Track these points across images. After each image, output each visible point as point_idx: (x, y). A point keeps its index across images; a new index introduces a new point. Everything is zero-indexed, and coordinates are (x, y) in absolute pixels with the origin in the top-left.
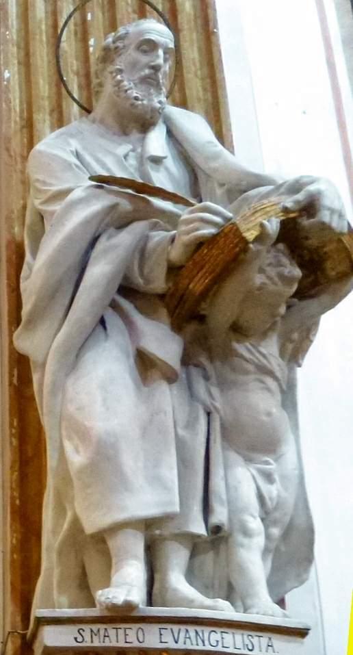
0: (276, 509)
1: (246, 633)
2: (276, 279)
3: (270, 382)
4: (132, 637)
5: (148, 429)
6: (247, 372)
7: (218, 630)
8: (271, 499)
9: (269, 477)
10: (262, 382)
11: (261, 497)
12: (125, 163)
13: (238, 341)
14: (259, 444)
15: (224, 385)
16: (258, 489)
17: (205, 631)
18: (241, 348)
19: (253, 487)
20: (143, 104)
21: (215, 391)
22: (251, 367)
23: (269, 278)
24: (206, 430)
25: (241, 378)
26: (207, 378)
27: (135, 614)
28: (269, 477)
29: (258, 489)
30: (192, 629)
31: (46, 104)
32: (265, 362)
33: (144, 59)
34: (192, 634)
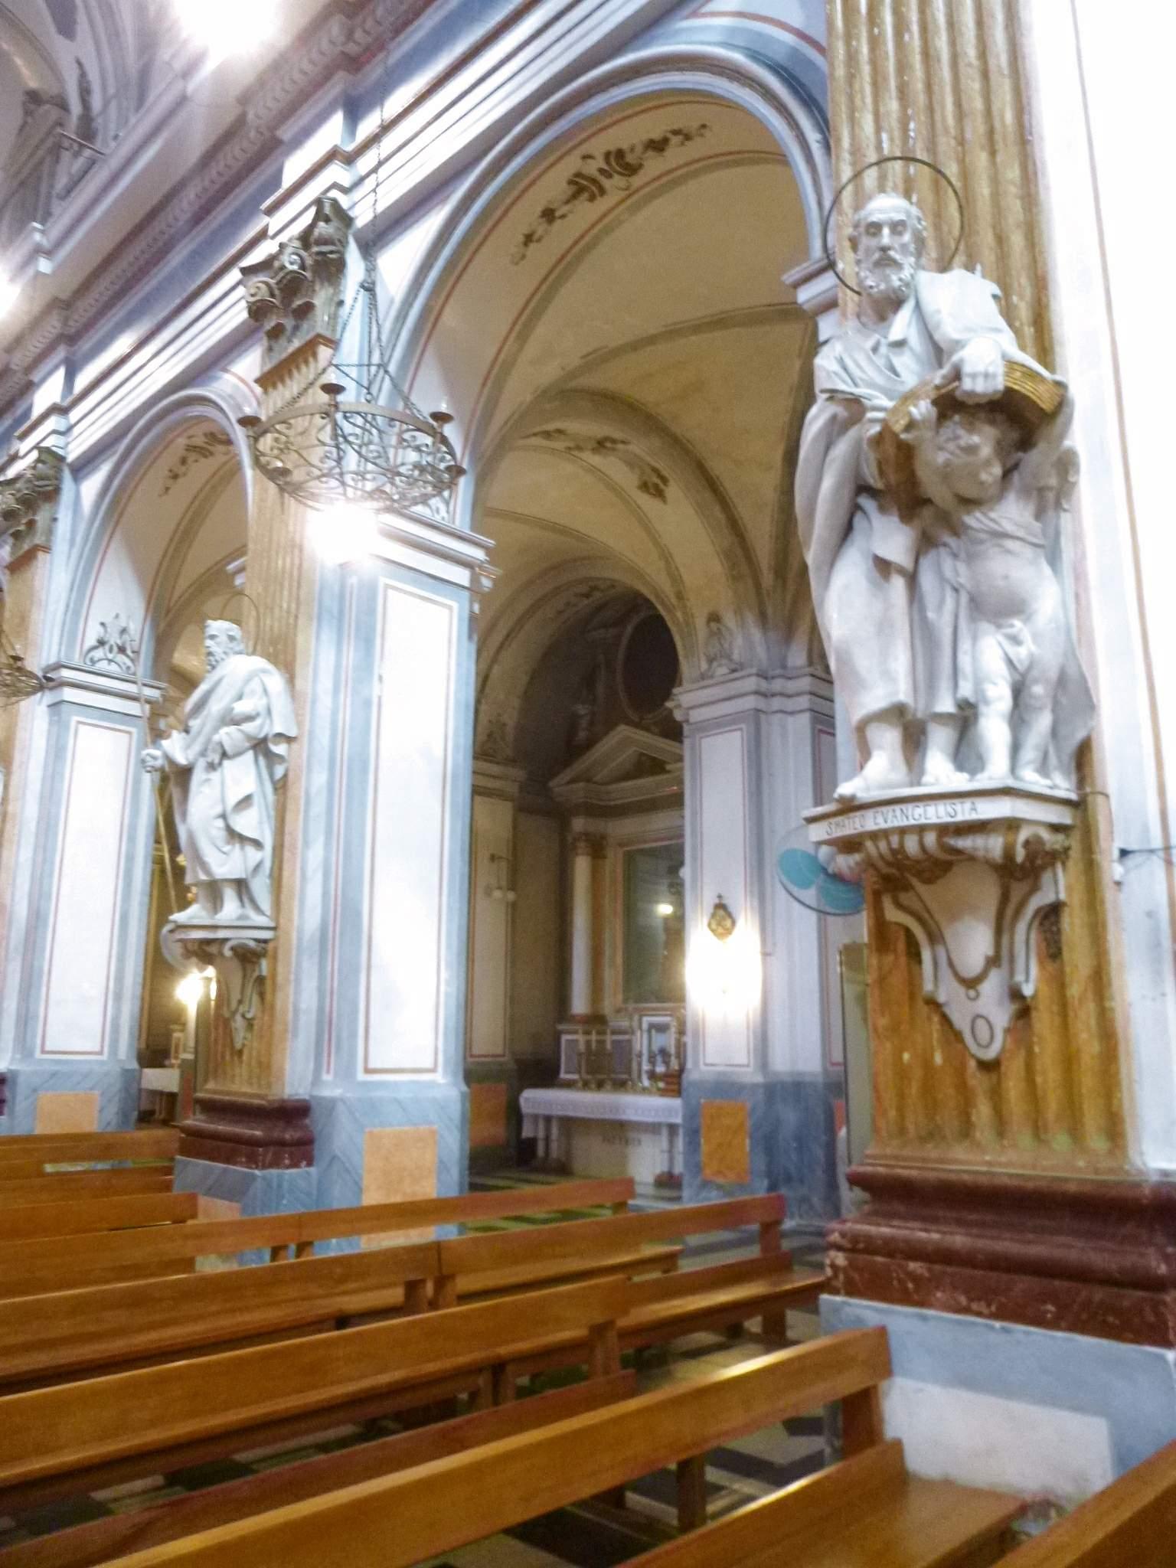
0: (1030, 668)
1: (948, 802)
2: (958, 452)
3: (1010, 544)
4: (880, 820)
5: (884, 627)
6: (982, 542)
7: (921, 804)
8: (1020, 660)
9: (1015, 640)
10: (1000, 546)
11: (1010, 662)
12: (874, 358)
13: (968, 513)
14: (996, 608)
15: (971, 558)
16: (1006, 655)
17: (909, 808)
18: (974, 520)
19: (1000, 652)
20: (881, 292)
21: (962, 568)
22: (983, 536)
23: (952, 453)
24: (289, 817)
25: (982, 547)
26: (955, 556)
27: (857, 803)
28: (1015, 640)
29: (1006, 655)
30: (897, 808)
31: (1013, 190)
32: (996, 527)
33: (873, 242)
34: (898, 813)
